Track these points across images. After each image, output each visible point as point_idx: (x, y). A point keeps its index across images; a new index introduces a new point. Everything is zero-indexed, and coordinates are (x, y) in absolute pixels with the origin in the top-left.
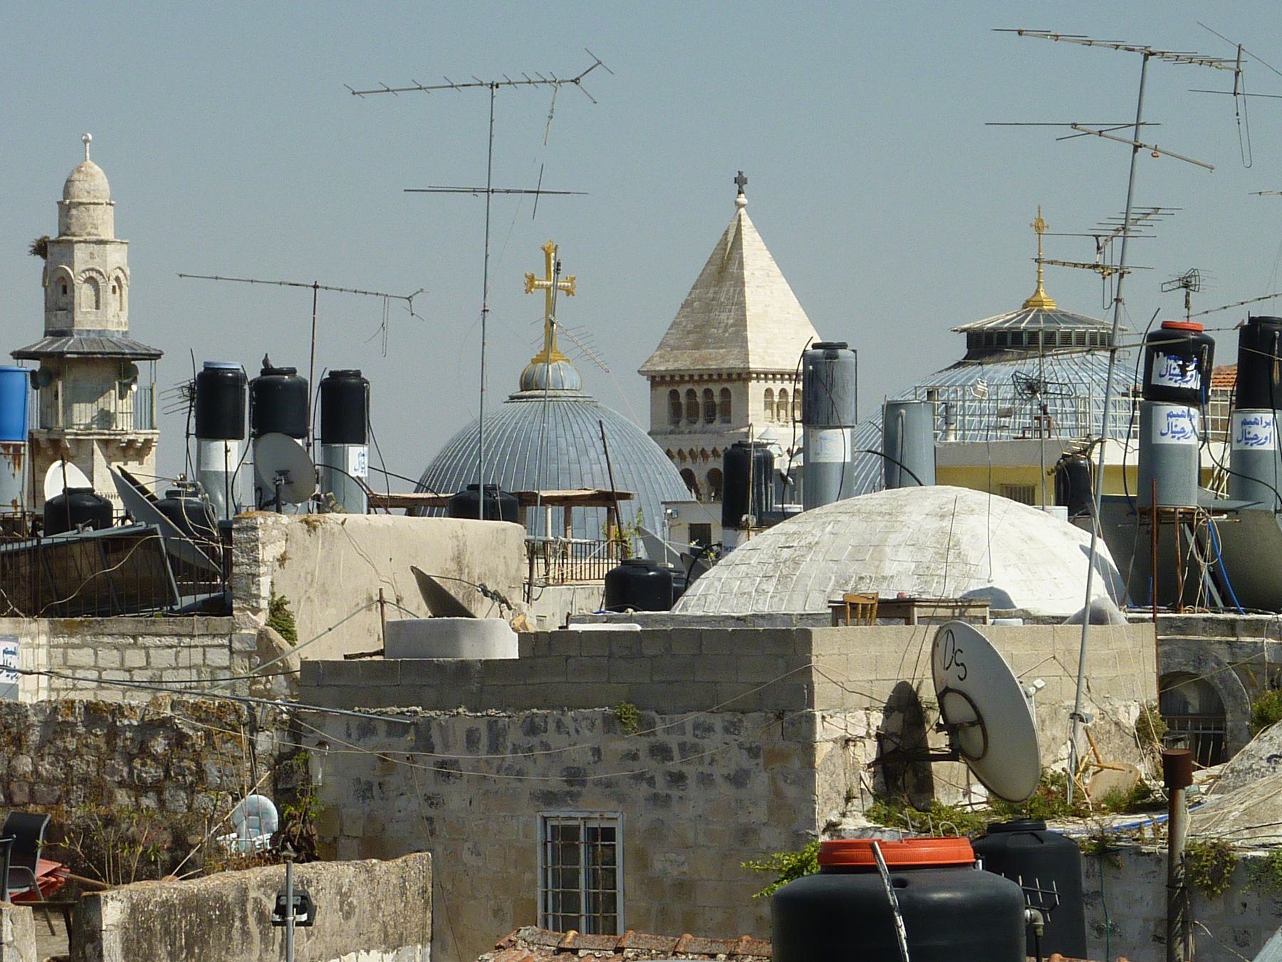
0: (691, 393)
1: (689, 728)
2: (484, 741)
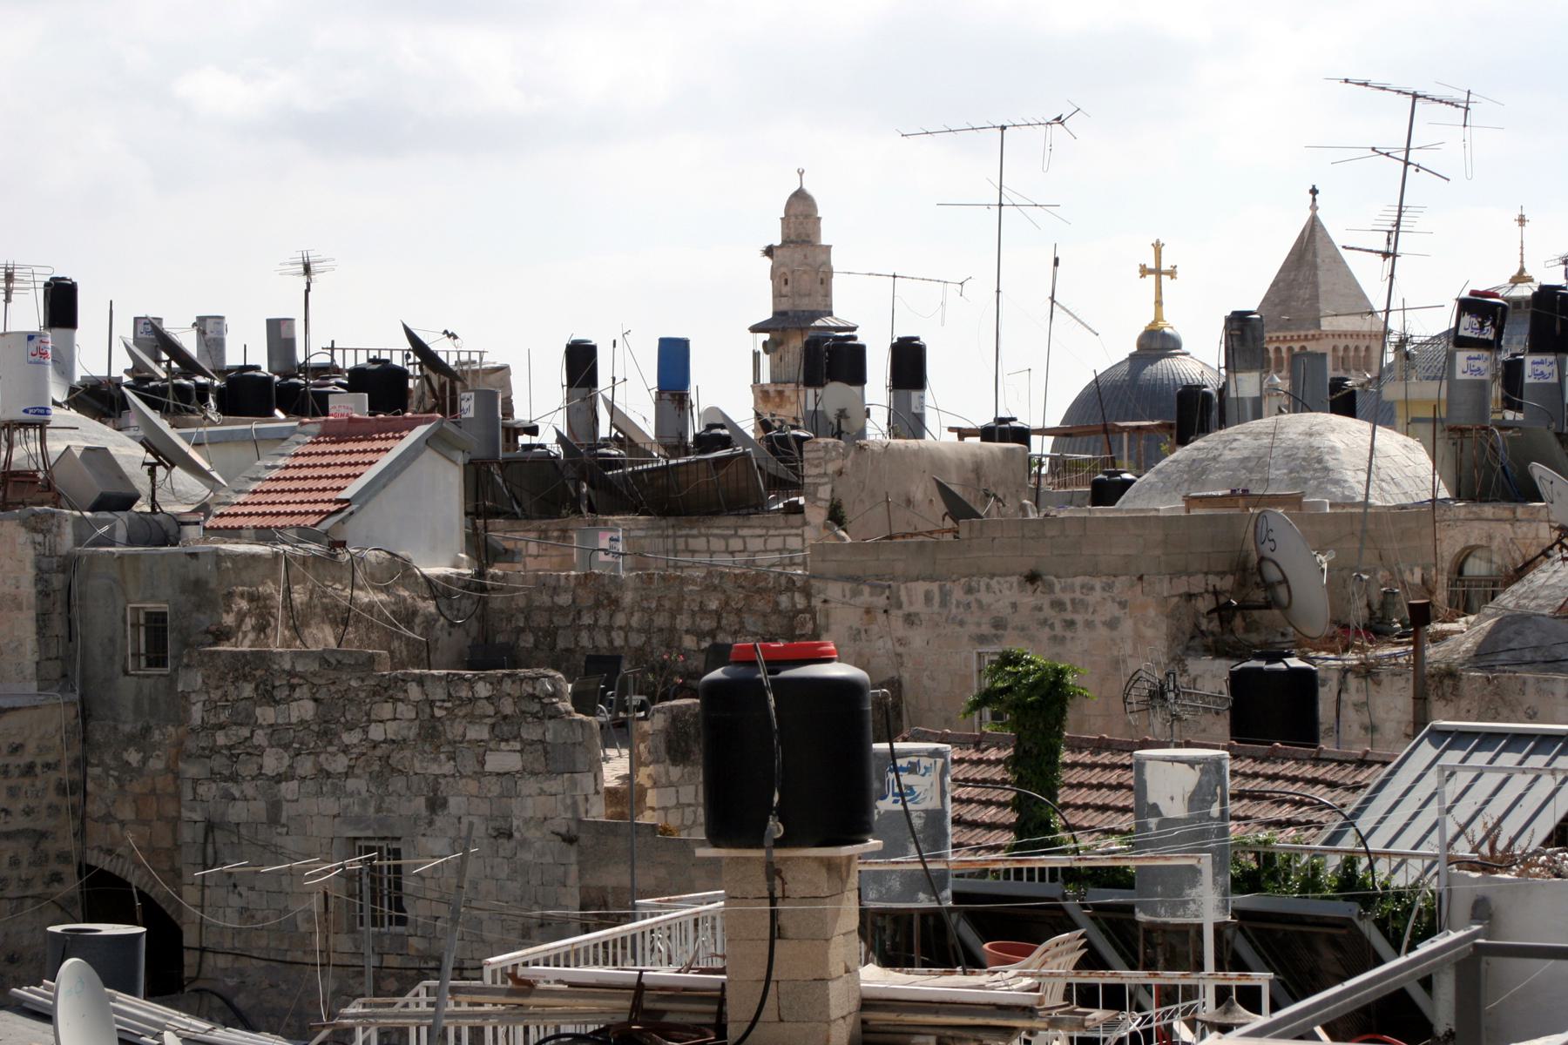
0: (1278, 350)
1: (1078, 589)
2: (937, 598)
